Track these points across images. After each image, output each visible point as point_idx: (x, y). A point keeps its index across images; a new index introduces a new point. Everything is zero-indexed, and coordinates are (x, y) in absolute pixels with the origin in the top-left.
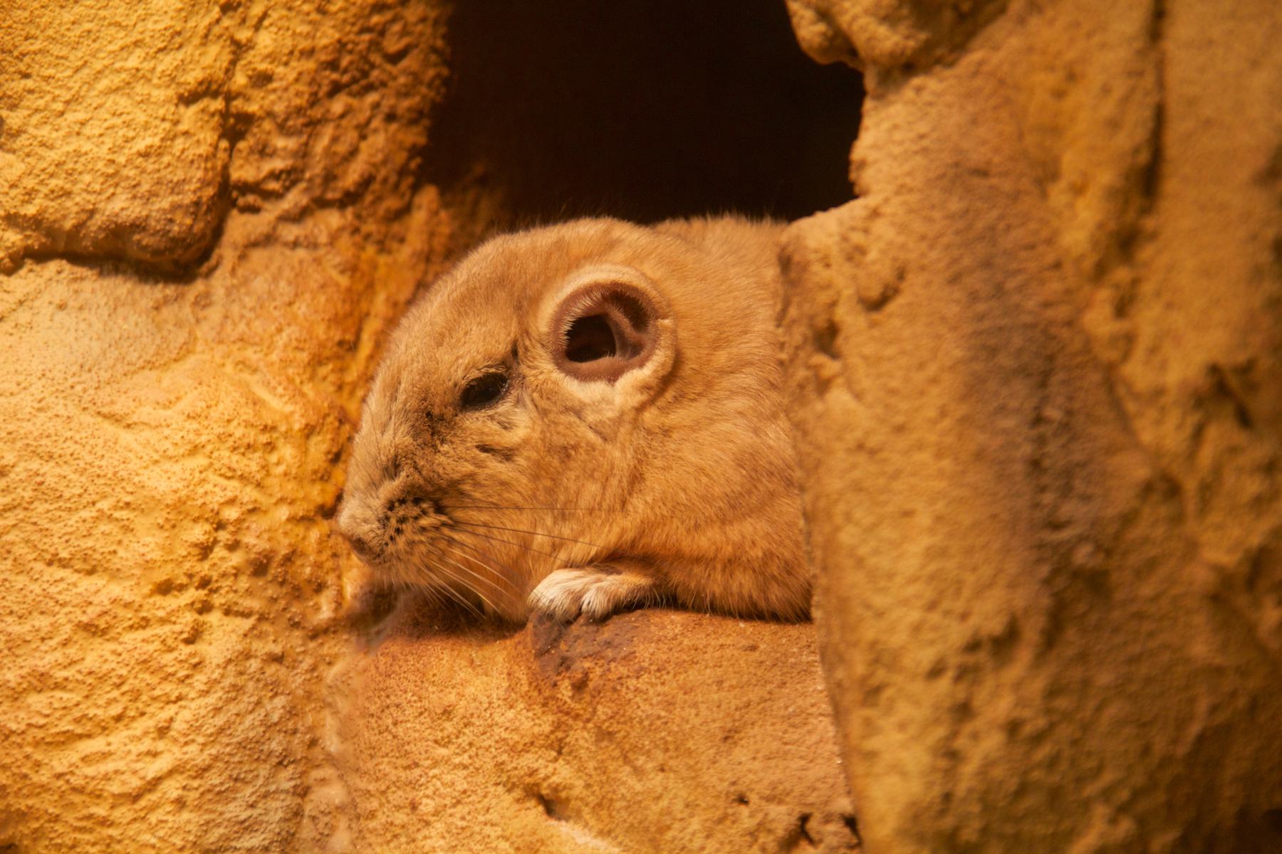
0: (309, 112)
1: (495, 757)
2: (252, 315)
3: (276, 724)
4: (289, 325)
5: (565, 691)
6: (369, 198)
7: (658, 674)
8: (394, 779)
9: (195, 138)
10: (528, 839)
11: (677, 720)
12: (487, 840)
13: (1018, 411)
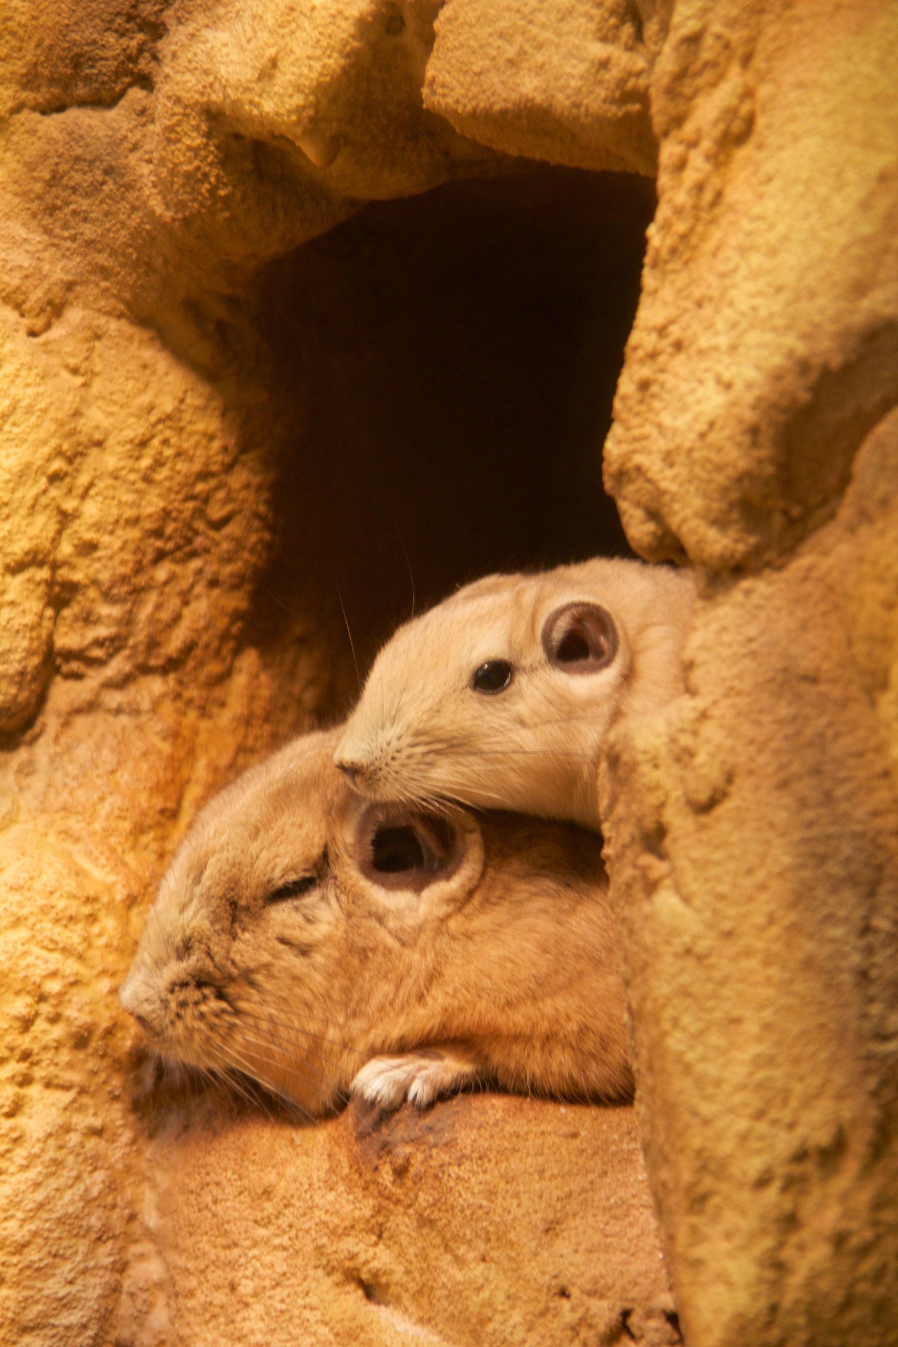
0: (133, 580)
1: (315, 1240)
2: (74, 784)
3: (95, 1199)
4: (111, 793)
5: (386, 1176)
6: (191, 664)
7: (480, 1162)
8: (213, 1257)
9: (21, 608)
10: (347, 1324)
11: (499, 1210)
12: (306, 1324)
13: (846, 920)
